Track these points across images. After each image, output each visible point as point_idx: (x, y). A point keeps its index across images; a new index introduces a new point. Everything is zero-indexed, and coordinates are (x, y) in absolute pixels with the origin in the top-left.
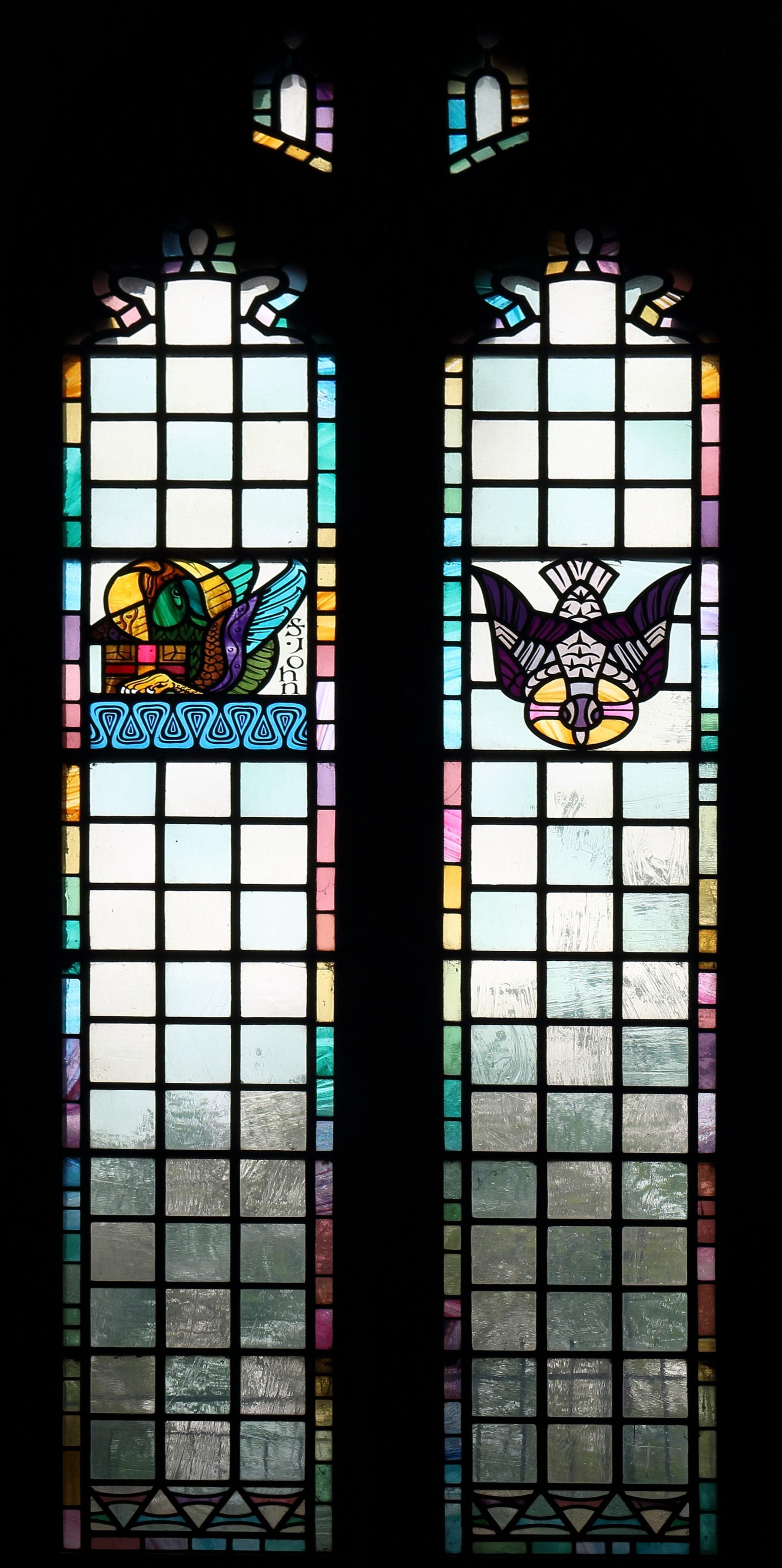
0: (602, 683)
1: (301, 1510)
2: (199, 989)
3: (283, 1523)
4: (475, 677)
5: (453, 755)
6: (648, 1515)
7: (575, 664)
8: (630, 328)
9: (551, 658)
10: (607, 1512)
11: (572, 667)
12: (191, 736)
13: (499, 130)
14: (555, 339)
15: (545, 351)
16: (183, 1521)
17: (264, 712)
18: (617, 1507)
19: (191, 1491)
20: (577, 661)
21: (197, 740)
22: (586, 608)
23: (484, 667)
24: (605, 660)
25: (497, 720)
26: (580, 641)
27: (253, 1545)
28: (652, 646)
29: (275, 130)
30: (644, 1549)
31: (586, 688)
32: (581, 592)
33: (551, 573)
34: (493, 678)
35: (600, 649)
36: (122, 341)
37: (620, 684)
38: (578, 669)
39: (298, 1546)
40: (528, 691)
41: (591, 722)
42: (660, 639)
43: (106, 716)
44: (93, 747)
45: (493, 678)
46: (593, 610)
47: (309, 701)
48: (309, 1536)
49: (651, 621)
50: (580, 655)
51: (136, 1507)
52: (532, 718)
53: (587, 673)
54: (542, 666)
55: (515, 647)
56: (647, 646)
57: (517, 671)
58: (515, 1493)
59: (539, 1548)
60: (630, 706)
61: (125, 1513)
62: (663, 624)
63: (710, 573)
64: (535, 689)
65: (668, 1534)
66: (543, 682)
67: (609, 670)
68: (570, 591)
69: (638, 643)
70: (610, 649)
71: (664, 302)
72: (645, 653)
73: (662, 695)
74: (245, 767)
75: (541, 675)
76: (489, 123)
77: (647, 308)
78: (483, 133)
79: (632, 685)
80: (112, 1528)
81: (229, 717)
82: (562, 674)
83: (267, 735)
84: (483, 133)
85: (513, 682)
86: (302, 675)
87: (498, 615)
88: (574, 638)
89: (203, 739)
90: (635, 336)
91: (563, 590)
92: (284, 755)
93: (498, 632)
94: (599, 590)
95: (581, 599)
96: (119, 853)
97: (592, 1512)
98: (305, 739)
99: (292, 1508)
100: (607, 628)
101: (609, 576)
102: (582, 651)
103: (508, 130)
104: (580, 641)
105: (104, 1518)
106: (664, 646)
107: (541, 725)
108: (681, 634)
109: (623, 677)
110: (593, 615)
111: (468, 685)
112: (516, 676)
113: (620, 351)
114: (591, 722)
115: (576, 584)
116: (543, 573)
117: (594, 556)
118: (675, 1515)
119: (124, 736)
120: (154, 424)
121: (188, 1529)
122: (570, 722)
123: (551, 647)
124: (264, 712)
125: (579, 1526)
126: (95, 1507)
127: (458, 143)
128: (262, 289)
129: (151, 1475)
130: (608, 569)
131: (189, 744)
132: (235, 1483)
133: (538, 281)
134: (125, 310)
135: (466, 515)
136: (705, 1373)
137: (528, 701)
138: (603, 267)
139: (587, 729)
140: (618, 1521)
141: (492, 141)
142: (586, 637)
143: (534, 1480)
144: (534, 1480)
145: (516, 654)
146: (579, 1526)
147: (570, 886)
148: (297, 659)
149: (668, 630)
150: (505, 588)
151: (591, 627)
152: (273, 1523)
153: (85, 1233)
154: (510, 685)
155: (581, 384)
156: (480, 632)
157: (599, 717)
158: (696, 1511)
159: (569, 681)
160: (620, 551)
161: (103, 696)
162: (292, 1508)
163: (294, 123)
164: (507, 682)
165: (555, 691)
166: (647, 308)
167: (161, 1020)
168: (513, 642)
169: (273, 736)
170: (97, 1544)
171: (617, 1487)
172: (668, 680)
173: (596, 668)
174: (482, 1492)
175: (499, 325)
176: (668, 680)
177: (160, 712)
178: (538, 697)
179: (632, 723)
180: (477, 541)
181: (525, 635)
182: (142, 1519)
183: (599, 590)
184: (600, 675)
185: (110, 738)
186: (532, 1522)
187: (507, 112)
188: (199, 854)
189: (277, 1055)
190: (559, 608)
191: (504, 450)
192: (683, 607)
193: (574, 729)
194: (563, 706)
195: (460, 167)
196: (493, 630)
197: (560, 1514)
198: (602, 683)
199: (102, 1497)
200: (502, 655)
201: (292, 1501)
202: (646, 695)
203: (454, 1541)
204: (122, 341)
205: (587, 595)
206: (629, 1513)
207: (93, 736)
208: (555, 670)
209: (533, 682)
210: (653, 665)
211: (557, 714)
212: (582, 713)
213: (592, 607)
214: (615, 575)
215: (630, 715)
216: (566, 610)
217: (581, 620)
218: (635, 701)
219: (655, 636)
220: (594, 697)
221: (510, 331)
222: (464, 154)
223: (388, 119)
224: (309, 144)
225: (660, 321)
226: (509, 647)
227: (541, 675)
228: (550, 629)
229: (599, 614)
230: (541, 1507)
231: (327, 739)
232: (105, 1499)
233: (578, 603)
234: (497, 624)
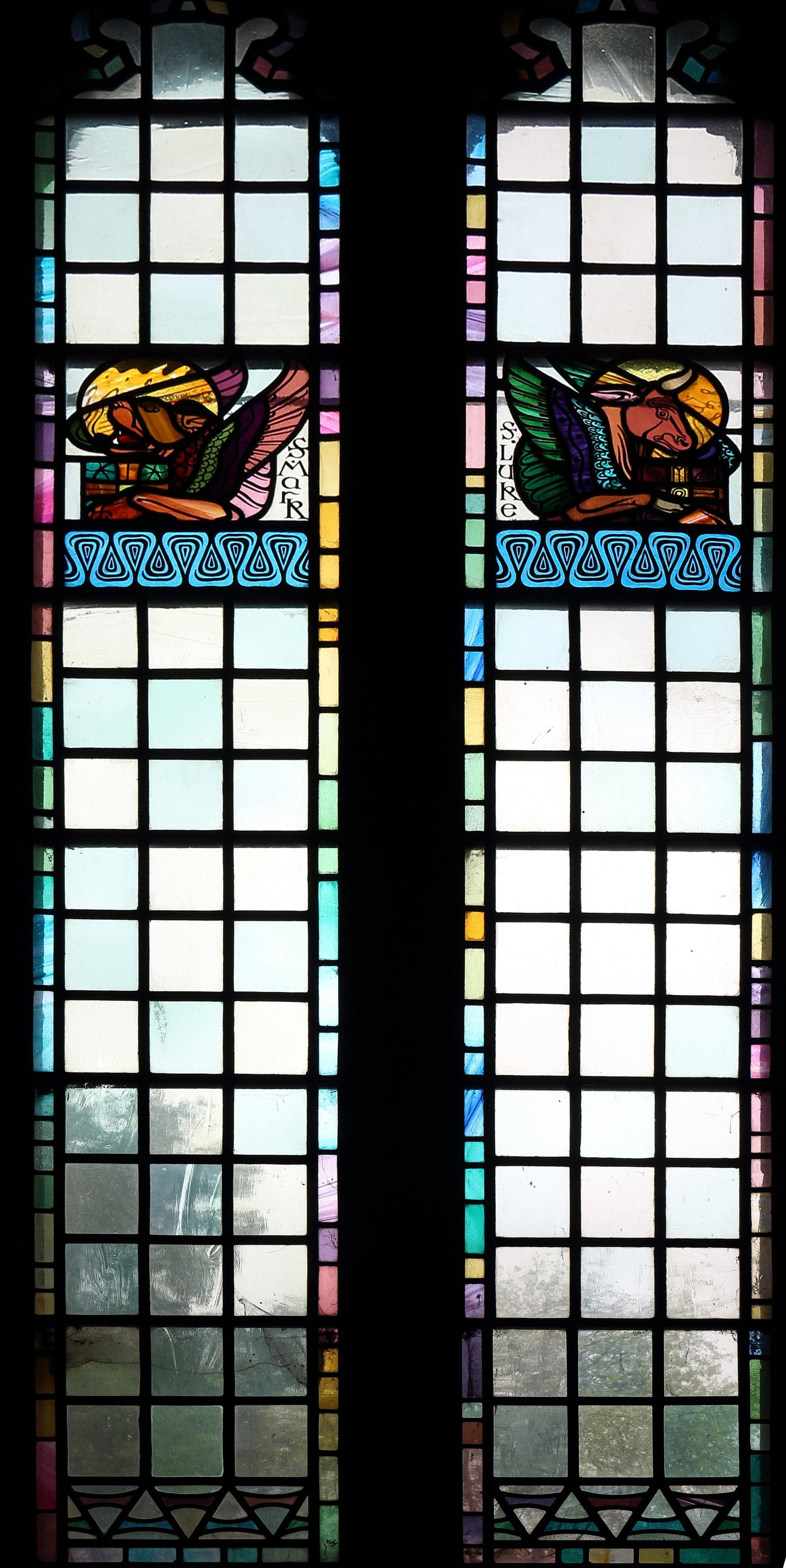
3: (284, 1528)
6: (605, 1516)
10: (560, 1514)
12: (611, 573)
16: (169, 1527)
17: (592, 541)
21: (618, 578)
27: (250, 1555)
36: (101, 95)
39: (300, 1555)
47: (311, 527)
51: (204, 1512)
58: (625, 1490)
77: (260, 59)
81: (654, 550)
83: (697, 573)
86: (302, 495)
89: (572, 576)
90: (246, 91)
96: (529, 715)
97: (287, 1511)
105: (84, 1525)
118: (292, 1516)
119: (685, 575)
121: (176, 1538)
125: (188, 1531)
126: (73, 1511)
129: (563, 1472)
132: (573, 1482)
133: (569, 25)
134: (107, 59)
135: (490, 306)
140: (573, 1525)
143: (650, 1475)
144: (650, 1475)
146: (188, 1531)
148: (300, 478)
153: (59, 1175)
161: (86, 523)
166: (260, 59)
169: (171, 569)
175: (96, 74)
177: (577, 543)
185: (88, 573)
186: (134, 1525)
188: (618, 716)
197: (594, 1517)
199: (81, 1499)
201: (291, 1501)
204: (101, 95)
207: (500, 573)
225: (272, 73)
230: (571, 1508)
231: (330, 573)
232: (85, 1501)
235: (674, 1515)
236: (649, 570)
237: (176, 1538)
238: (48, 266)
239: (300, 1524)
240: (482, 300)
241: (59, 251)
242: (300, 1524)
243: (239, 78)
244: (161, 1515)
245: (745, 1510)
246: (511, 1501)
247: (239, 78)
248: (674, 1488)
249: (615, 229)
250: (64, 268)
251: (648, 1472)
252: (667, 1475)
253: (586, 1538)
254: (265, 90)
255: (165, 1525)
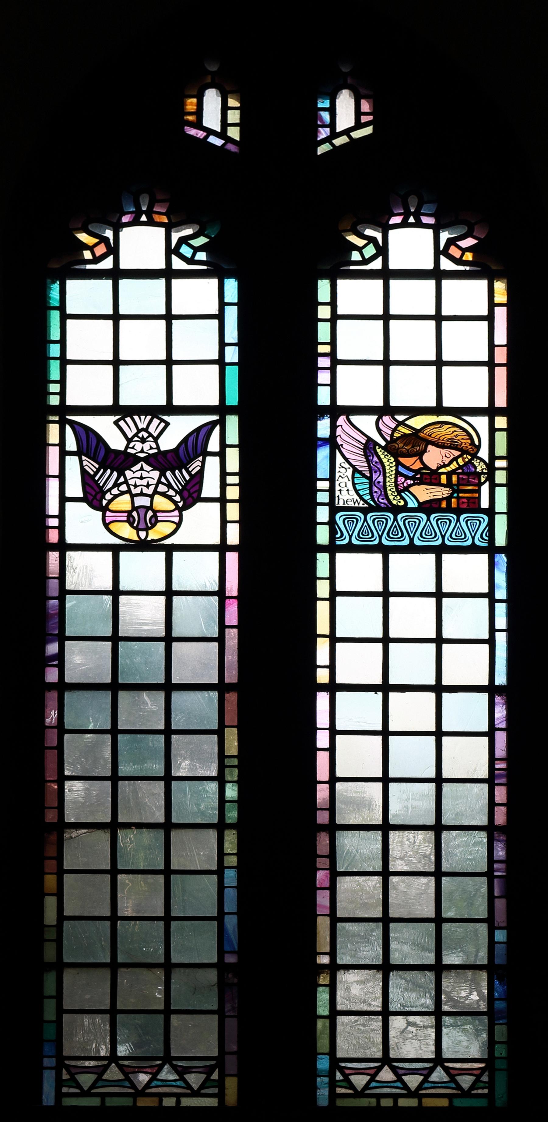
0: (157, 497)
1: (215, 1076)
2: (412, 711)
4: (68, 494)
5: (232, 548)
7: (138, 484)
8: (175, 259)
9: (122, 479)
10: (106, 1077)
11: (136, 486)
13: (353, 124)
14: (124, 265)
15: (386, 275)
18: (438, 1075)
19: (407, 1065)
20: (139, 482)
22: (146, 446)
23: (74, 487)
24: (159, 482)
25: (83, 523)
26: (142, 469)
28: (193, 473)
29: (198, 124)
30: (186, 1102)
31: (144, 501)
32: (143, 436)
33: (122, 423)
34: (80, 495)
35: (156, 474)
37: (170, 498)
38: (140, 487)
40: (104, 502)
41: (149, 525)
42: (199, 468)
43: (348, 521)
44: (338, 543)
45: (80, 495)
46: (151, 448)
48: (221, 1096)
49: (192, 456)
50: (141, 478)
52: (107, 522)
53: (145, 491)
54: (116, 485)
55: (96, 473)
56: (189, 473)
57: (98, 490)
59: (110, 1102)
60: (176, 513)
61: (360, 1081)
62: (200, 458)
63: (232, 422)
64: (110, 501)
65: (474, 1092)
66: (116, 496)
67: (162, 488)
68: (136, 435)
69: (184, 471)
70: (163, 474)
71: (469, 242)
72: (188, 477)
73: (199, 505)
74: (445, 557)
75: (115, 491)
76: (345, 119)
78: (340, 127)
79: (178, 498)
80: (78, 1091)
82: (129, 491)
83: (431, 535)
84: (340, 127)
85: (95, 497)
87: (85, 451)
88: (138, 467)
90: (446, 264)
91: (130, 436)
92: (473, 549)
93: (85, 463)
94: (155, 435)
95: (143, 441)
96: (357, 617)
98: (487, 538)
99: (478, 1077)
100: (162, 461)
101: (163, 425)
102: (143, 476)
103: (359, 125)
104: (142, 469)
106: (201, 473)
107: (113, 527)
108: (212, 464)
109: (171, 493)
110: (151, 452)
111: (63, 499)
112: (97, 493)
113: (437, 275)
114: (149, 525)
115: (139, 431)
116: (116, 423)
117: (153, 411)
118: (207, 1079)
120: (111, 322)
121: (132, 1091)
122: (135, 525)
123: (121, 473)
124: (395, 519)
127: (324, 133)
128: (189, 232)
130: (162, 420)
131: (406, 542)
132: (386, 1060)
136: (231, 978)
137: (104, 510)
138: (157, 218)
139: (147, 529)
141: (347, 132)
142: (146, 467)
144: (432, 1055)
145: (97, 478)
147: (407, 639)
149: (203, 462)
150: (91, 434)
151: (150, 460)
152: (196, 1087)
154: (92, 500)
155: (142, 296)
156: (72, 463)
157: (155, 521)
158: (331, 1075)
159: (133, 496)
160: (171, 409)
162: (209, 1073)
163: (212, 119)
164: (90, 498)
165: (123, 503)
167: (385, 733)
168: (95, 470)
170: (339, 1102)
171: (386, 1060)
172: (203, 495)
173: (152, 488)
174: (342, 1064)
176: (203, 495)
178: (112, 507)
179: (179, 525)
180: (70, 401)
181: (103, 465)
182: (373, 1084)
183: (155, 435)
184: (155, 492)
187: (358, 113)
189: (468, 758)
190: (127, 447)
191: (87, 340)
192: (214, 445)
193: (138, 529)
194: (129, 513)
195: (323, 149)
196: (81, 461)
197: (182, 1079)
198: (157, 497)
200: (87, 479)
202: (187, 506)
203: (48, 1098)
204: (89, 267)
205: (148, 437)
206: (395, 1078)
208: (124, 488)
209: (108, 496)
210: (194, 486)
211: (125, 519)
212: (142, 518)
213: (151, 447)
214: (167, 424)
215: (176, 519)
216: (133, 448)
217: (142, 455)
218: (181, 510)
219: (195, 466)
220: (151, 508)
221: (96, 260)
222: (328, 140)
223: (280, 117)
224: (222, 134)
226: (92, 473)
227: (115, 491)
228: (121, 462)
229: (156, 451)
233: (140, 444)
234: (84, 458)
235: (124, 1078)
236: (431, 535)
237: (132, 1091)
238: (55, 316)
239: (482, 1085)
240: (228, 349)
241: (62, 307)
242: (482, 1085)
243: (442, 257)
244: (76, 1076)
245: (491, 1077)
246: (73, 1071)
247: (442, 257)
248: (121, 1062)
249: (410, 330)
250: (65, 317)
251: (379, 1055)
252: (173, 1054)
253: (394, 1091)
254: (458, 264)
255: (399, 1084)
